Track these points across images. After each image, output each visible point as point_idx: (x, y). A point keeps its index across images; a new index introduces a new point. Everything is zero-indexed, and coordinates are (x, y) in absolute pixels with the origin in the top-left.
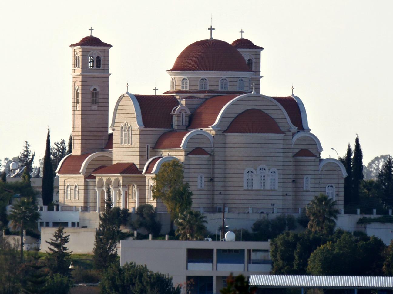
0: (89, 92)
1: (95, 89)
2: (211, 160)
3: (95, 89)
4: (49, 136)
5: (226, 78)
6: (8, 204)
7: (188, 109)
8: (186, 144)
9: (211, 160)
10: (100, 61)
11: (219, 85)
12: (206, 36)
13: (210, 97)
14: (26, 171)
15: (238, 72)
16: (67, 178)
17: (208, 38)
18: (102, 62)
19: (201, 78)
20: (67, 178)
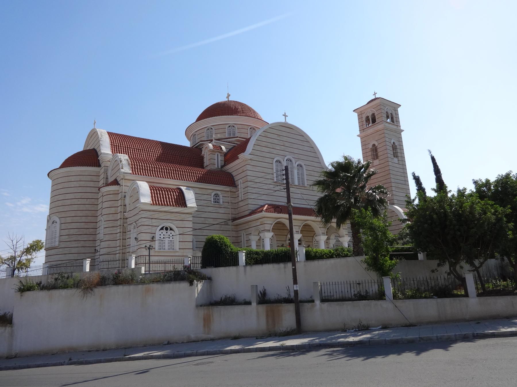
0: (368, 150)
1: (374, 145)
2: (295, 282)
3: (374, 145)
4: (433, 159)
5: (234, 125)
6: (342, 208)
7: (315, 231)
8: (175, 187)
9: (295, 282)
10: (393, 118)
11: (226, 132)
12: (282, 120)
13: (210, 141)
14: (419, 196)
15: (214, 118)
16: (208, 225)
17: (283, 121)
18: (395, 119)
19: (228, 125)
20: (208, 225)
